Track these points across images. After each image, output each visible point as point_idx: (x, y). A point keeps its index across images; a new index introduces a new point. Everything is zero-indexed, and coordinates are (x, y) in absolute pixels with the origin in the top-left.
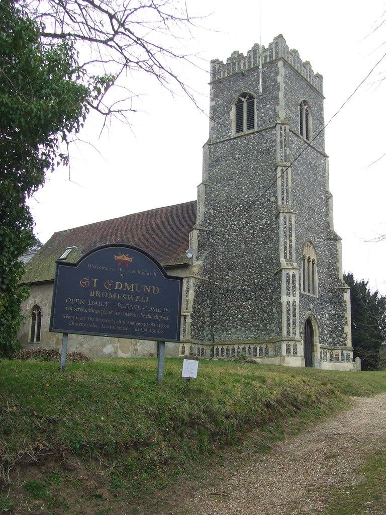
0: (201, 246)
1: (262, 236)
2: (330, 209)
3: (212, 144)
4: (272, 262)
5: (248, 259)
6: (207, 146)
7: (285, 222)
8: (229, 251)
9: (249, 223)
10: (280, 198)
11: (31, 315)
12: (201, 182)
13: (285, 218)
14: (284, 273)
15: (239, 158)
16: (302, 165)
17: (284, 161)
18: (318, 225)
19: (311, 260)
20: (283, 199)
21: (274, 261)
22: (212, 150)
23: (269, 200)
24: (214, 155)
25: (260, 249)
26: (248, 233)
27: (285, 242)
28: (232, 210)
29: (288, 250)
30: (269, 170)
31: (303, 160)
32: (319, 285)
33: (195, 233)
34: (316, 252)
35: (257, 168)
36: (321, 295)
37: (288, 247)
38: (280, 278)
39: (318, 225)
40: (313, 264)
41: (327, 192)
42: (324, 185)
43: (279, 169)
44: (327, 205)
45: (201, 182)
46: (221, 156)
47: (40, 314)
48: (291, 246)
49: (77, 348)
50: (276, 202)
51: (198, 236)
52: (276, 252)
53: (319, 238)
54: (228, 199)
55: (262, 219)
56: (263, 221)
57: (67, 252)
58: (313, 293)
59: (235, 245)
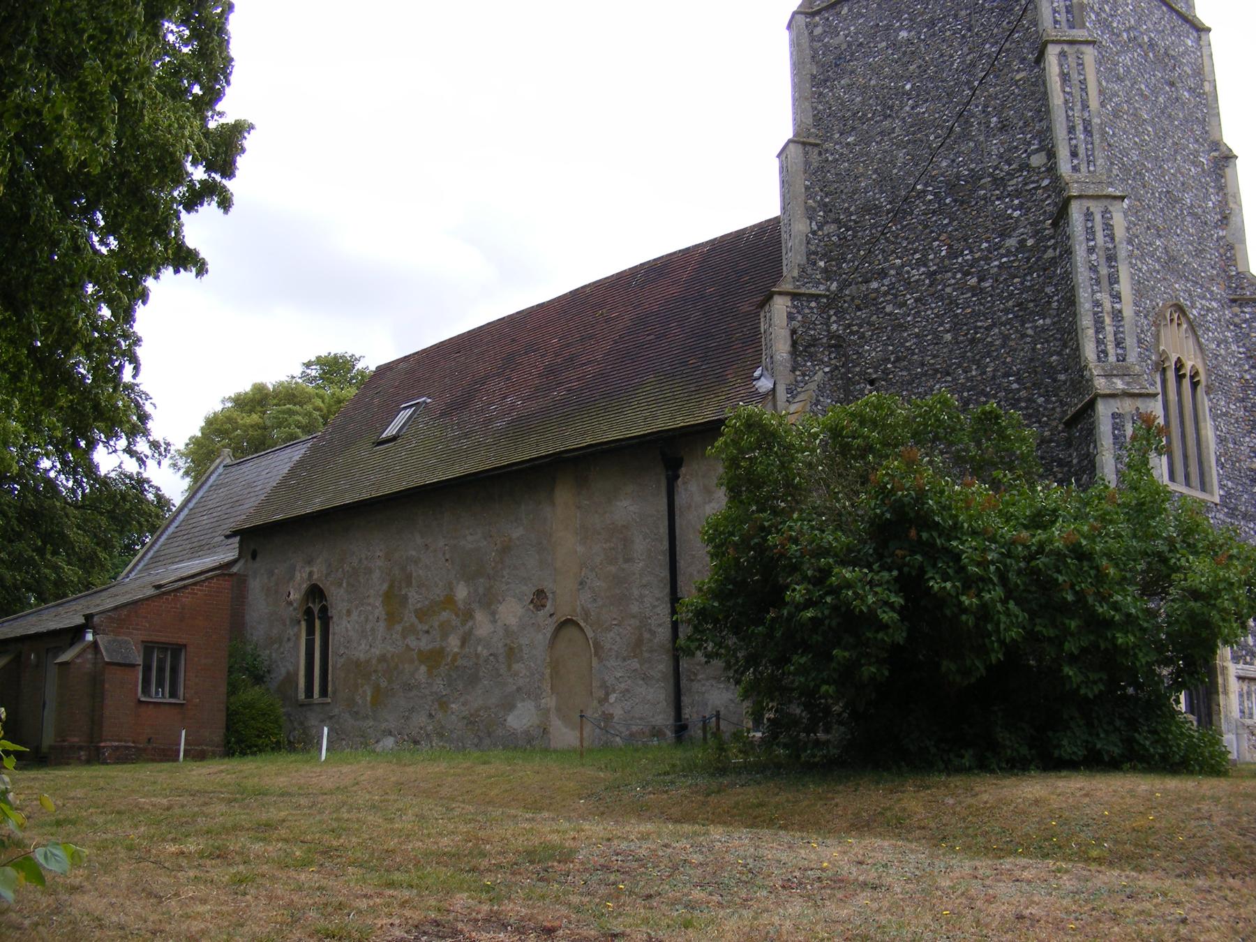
0: (802, 348)
1: (1011, 295)
2: (1230, 199)
3: (818, 12)
4: (1055, 380)
5: (967, 379)
6: (801, 20)
7: (1090, 233)
8: (898, 359)
9: (962, 254)
10: (1063, 153)
11: (300, 615)
12: (790, 135)
13: (1089, 216)
14: (1104, 410)
15: (909, 42)
16: (1125, 48)
17: (1064, 24)
18: (1199, 253)
19: (1187, 370)
20: (1074, 154)
21: (1062, 377)
22: (818, 31)
23: (1025, 166)
24: (825, 45)
25: (1006, 338)
26: (962, 287)
27: (1097, 304)
28: (898, 214)
29: (1109, 329)
30: (1016, 65)
31: (1128, 30)
32: (1218, 460)
33: (780, 306)
34: (1198, 340)
35: (973, 65)
36: (1228, 495)
37: (1108, 320)
38: (1090, 434)
39: (1199, 253)
40: (1195, 385)
41: (1217, 145)
42: (1203, 122)
43: (1052, 52)
44: (1221, 188)
45: (789, 134)
46: (850, 45)
47: (324, 610)
48: (1117, 315)
49: (430, 716)
50: (1052, 169)
51: (791, 317)
52: (1065, 346)
53: (1204, 298)
54: (883, 180)
55: (1004, 235)
56: (1012, 242)
57: (404, 415)
58: (1203, 487)
59: (917, 336)
